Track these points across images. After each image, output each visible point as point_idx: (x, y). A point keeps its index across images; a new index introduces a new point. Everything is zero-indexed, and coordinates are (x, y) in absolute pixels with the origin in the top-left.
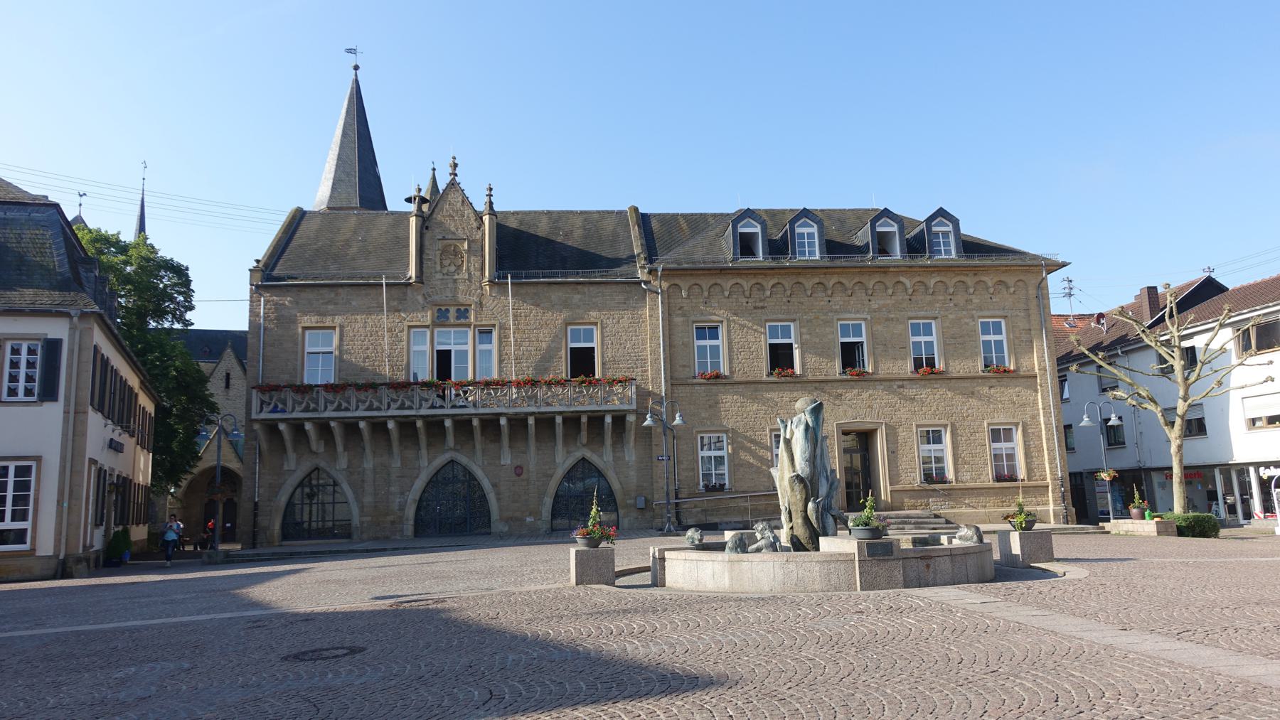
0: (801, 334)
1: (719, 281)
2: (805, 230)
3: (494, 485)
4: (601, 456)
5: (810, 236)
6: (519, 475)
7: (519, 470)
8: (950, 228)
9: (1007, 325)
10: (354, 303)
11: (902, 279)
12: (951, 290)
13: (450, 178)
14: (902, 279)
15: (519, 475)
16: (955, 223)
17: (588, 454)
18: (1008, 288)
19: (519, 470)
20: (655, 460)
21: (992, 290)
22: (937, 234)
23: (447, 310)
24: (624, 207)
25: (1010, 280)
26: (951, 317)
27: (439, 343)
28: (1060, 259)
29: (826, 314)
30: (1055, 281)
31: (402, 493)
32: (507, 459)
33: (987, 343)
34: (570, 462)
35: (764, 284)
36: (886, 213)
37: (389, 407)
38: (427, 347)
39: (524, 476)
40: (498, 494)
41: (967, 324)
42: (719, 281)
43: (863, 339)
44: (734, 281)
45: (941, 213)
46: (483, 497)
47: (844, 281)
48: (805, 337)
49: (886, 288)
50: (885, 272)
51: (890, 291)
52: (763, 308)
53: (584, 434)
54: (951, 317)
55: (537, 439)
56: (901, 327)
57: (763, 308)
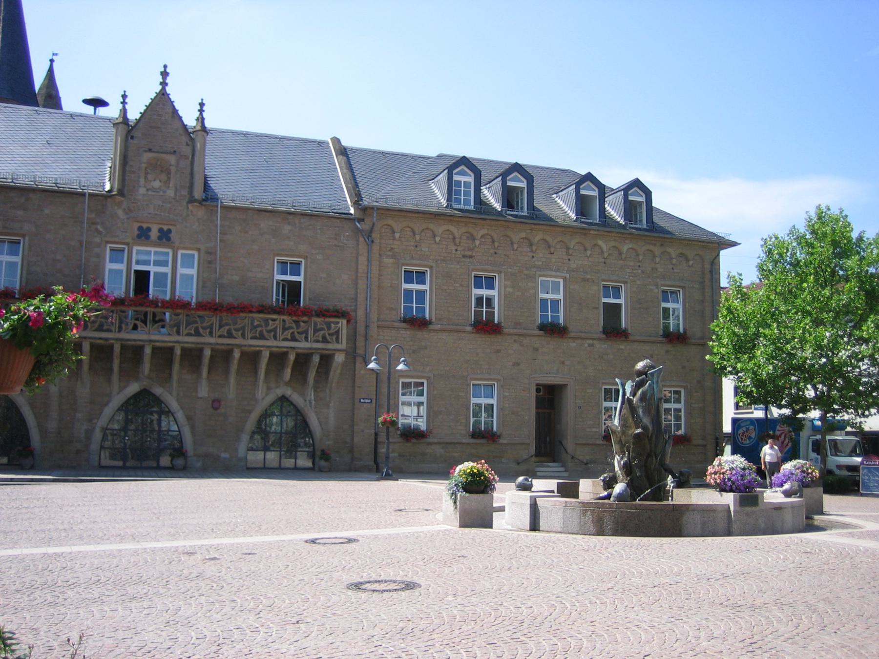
0: (506, 287)
1: (431, 226)
2: (462, 179)
3: (189, 418)
4: (302, 394)
5: (467, 184)
6: (216, 409)
7: (216, 404)
8: (642, 199)
9: (684, 294)
10: (47, 211)
11: (600, 242)
12: (641, 257)
13: (160, 87)
14: (600, 242)
15: (216, 409)
16: (648, 193)
17: (288, 392)
18: (687, 260)
19: (216, 404)
20: (357, 401)
21: (674, 261)
22: (459, 183)
23: (149, 229)
24: (326, 137)
25: (690, 254)
26: (638, 282)
27: (138, 263)
28: (732, 238)
29: (527, 269)
30: (725, 255)
31: (90, 421)
32: (203, 391)
33: (408, 292)
34: (271, 398)
35: (475, 233)
36: (589, 177)
37: (135, 328)
38: (122, 267)
39: (222, 410)
40: (193, 427)
41: (651, 290)
42: (431, 226)
43: (621, 301)
44: (446, 227)
45: (637, 184)
46: (23, 421)
47: (548, 239)
48: (508, 289)
49: (586, 250)
50: (585, 234)
51: (589, 253)
52: (471, 257)
53: (288, 372)
54: (638, 282)
55: (238, 373)
56: (595, 288)
57: (471, 257)
